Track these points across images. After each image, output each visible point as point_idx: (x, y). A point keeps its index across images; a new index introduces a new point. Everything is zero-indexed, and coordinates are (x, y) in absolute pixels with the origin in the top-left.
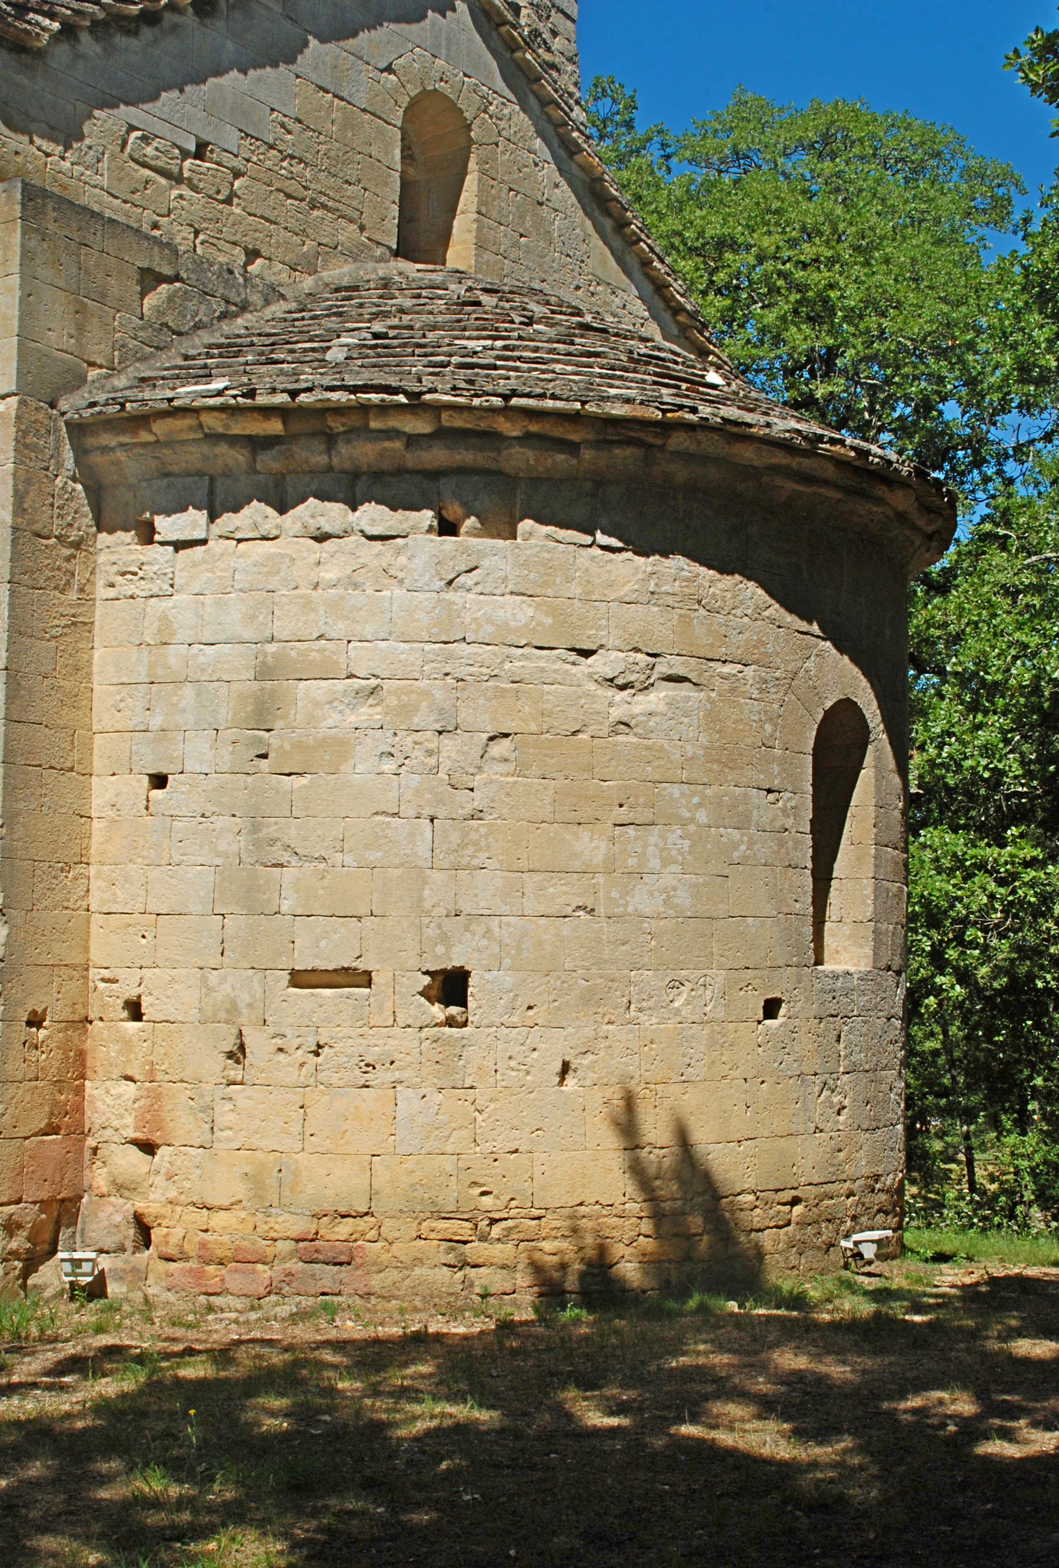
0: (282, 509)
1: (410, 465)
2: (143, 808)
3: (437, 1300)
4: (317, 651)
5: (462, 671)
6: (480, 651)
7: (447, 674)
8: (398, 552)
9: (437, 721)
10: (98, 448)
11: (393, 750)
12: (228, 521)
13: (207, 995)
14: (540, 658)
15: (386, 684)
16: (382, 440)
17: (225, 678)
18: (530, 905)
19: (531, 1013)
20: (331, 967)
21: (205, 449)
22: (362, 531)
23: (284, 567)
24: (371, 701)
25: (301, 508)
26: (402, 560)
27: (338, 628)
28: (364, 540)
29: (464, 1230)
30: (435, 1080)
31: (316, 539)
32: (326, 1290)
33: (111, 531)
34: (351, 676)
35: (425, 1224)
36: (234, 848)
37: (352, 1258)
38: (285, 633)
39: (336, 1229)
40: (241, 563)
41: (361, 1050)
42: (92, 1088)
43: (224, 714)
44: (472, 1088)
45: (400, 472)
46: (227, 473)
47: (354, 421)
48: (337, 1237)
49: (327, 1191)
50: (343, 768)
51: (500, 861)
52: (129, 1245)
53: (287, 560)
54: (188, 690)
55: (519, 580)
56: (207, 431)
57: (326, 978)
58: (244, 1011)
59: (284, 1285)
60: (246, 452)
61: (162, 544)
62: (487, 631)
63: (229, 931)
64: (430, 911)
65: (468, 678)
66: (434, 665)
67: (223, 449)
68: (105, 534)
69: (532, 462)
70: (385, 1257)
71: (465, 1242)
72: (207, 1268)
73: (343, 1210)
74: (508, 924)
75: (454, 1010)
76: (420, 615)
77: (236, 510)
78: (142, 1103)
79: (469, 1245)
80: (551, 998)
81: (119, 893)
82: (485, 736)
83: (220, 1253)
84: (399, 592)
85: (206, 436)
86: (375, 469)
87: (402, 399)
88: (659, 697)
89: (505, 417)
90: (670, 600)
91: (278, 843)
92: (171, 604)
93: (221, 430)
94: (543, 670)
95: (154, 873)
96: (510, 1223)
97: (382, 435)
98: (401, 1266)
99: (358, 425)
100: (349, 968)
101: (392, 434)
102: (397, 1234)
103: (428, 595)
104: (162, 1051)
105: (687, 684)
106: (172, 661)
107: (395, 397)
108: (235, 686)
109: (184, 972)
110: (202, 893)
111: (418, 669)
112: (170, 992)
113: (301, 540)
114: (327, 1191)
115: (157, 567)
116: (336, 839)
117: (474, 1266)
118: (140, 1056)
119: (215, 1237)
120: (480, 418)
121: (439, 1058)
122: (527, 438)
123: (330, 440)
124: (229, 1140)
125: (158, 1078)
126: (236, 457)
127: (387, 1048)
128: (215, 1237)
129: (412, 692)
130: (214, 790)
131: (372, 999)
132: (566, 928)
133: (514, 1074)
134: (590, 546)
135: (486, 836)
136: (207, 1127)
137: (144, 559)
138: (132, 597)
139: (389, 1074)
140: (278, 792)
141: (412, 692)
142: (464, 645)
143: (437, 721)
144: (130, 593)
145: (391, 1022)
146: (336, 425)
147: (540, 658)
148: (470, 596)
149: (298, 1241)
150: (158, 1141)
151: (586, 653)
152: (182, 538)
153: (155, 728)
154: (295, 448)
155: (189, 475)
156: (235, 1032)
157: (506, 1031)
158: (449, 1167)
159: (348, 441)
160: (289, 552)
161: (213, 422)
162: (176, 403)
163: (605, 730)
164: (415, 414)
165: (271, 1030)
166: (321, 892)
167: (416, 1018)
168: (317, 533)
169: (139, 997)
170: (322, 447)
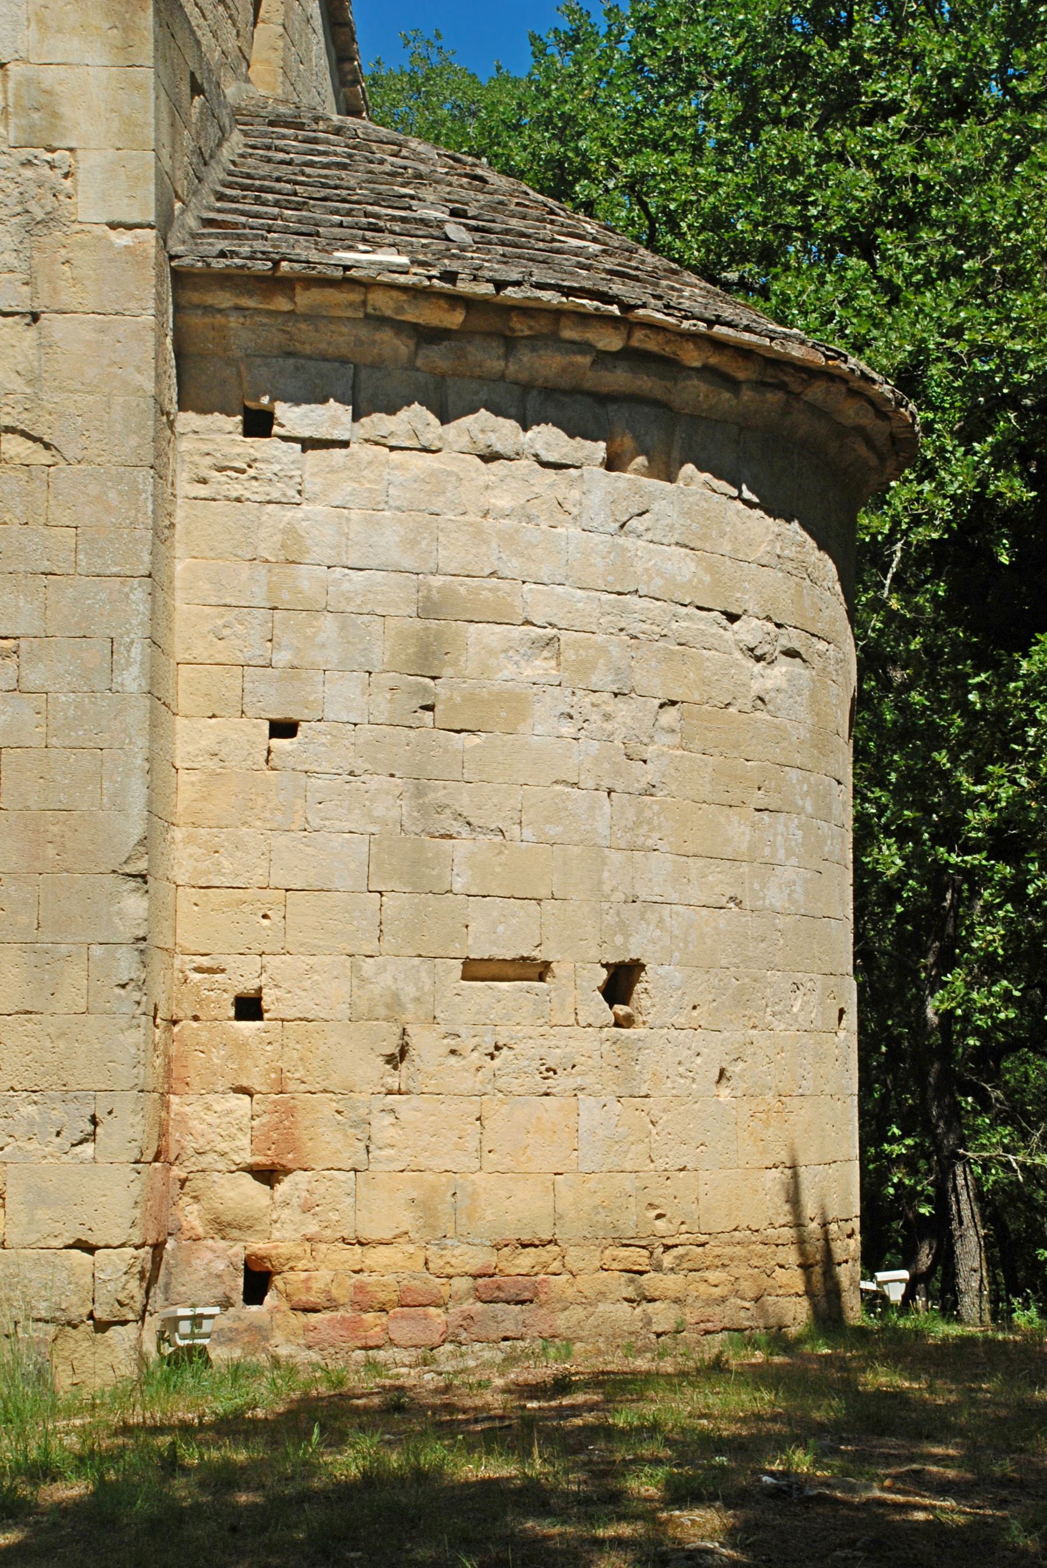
0: (445, 419)
1: (588, 385)
2: (262, 760)
3: (619, 1340)
4: (490, 590)
5: (636, 628)
6: (651, 606)
7: (621, 630)
8: (571, 485)
9: (614, 682)
10: (197, 307)
11: (572, 712)
12: (379, 423)
13: (359, 988)
14: (701, 619)
15: (564, 636)
16: (575, 353)
17: (379, 611)
18: (696, 895)
19: (695, 1013)
20: (509, 956)
21: (363, 333)
22: (536, 456)
23: (450, 487)
24: (545, 654)
25: (471, 418)
26: (575, 494)
27: (512, 566)
28: (537, 466)
29: (638, 1257)
30: (615, 1087)
31: (482, 457)
32: (509, 1334)
33: (203, 410)
34: (527, 622)
35: (607, 1252)
36: (395, 813)
37: (536, 1295)
38: (453, 565)
39: (517, 1262)
40: (398, 476)
41: (543, 1052)
42: (181, 1104)
43: (380, 653)
44: (647, 1096)
45: (576, 391)
46: (376, 366)
47: (542, 325)
48: (518, 1271)
49: (508, 1217)
50: (521, 728)
51: (670, 843)
52: (238, 1297)
53: (454, 479)
54: (328, 624)
55: (683, 529)
56: (370, 310)
57: (494, 969)
58: (410, 1006)
59: (461, 1330)
60: (411, 343)
61: (285, 439)
62: (656, 586)
63: (388, 911)
64: (609, 896)
65: (640, 635)
66: (609, 618)
67: (386, 335)
68: (191, 415)
69: (701, 398)
70: (570, 1292)
71: (641, 1273)
72: (365, 1316)
73: (526, 1238)
74: (677, 914)
75: (621, 1009)
76: (596, 559)
77: (391, 410)
78: (265, 1119)
79: (646, 1276)
80: (710, 997)
81: (226, 863)
82: (657, 702)
83: (382, 1296)
84: (574, 531)
85: (367, 316)
86: (550, 385)
87: (615, 309)
88: (785, 667)
89: (695, 344)
90: (789, 566)
91: (448, 811)
92: (300, 515)
93: (389, 313)
94: (703, 633)
95: (281, 841)
96: (680, 1250)
97: (574, 347)
98: (588, 1302)
99: (545, 331)
100: (528, 958)
101: (584, 347)
102: (581, 1265)
103: (603, 537)
104: (296, 1055)
105: (798, 660)
106: (305, 585)
107: (610, 307)
108: (391, 622)
109: (327, 959)
110: (352, 866)
111: (595, 620)
112: (307, 984)
113: (468, 457)
114: (508, 1217)
115: (279, 467)
116: (514, 809)
117: (649, 1301)
118: (262, 1062)
119: (375, 1277)
120: (668, 342)
121: (618, 1061)
122: (706, 371)
123: (510, 343)
124: (390, 1160)
125: (290, 1088)
126: (401, 347)
127: (568, 1049)
128: (375, 1277)
129: (590, 647)
130: (367, 743)
131: (553, 994)
132: (721, 919)
133: (682, 1081)
134: (735, 498)
135: (658, 814)
136: (361, 1145)
137: (258, 455)
138: (238, 500)
139: (571, 1080)
140: (446, 751)
141: (590, 647)
142: (635, 598)
143: (614, 682)
144: (235, 494)
145: (572, 1021)
146: (521, 327)
147: (701, 619)
148: (641, 543)
149: (475, 1277)
150: (290, 1166)
151: (733, 618)
152: (317, 435)
153: (281, 664)
154: (470, 348)
155: (325, 359)
156: (399, 1031)
157: (676, 1033)
158: (629, 1188)
159: (533, 350)
160: (455, 469)
161: (382, 302)
162: (353, 273)
163: (748, 708)
164: (616, 328)
165: (442, 1029)
166: (498, 869)
167: (597, 1016)
168: (485, 451)
169: (260, 989)
170: (501, 351)
